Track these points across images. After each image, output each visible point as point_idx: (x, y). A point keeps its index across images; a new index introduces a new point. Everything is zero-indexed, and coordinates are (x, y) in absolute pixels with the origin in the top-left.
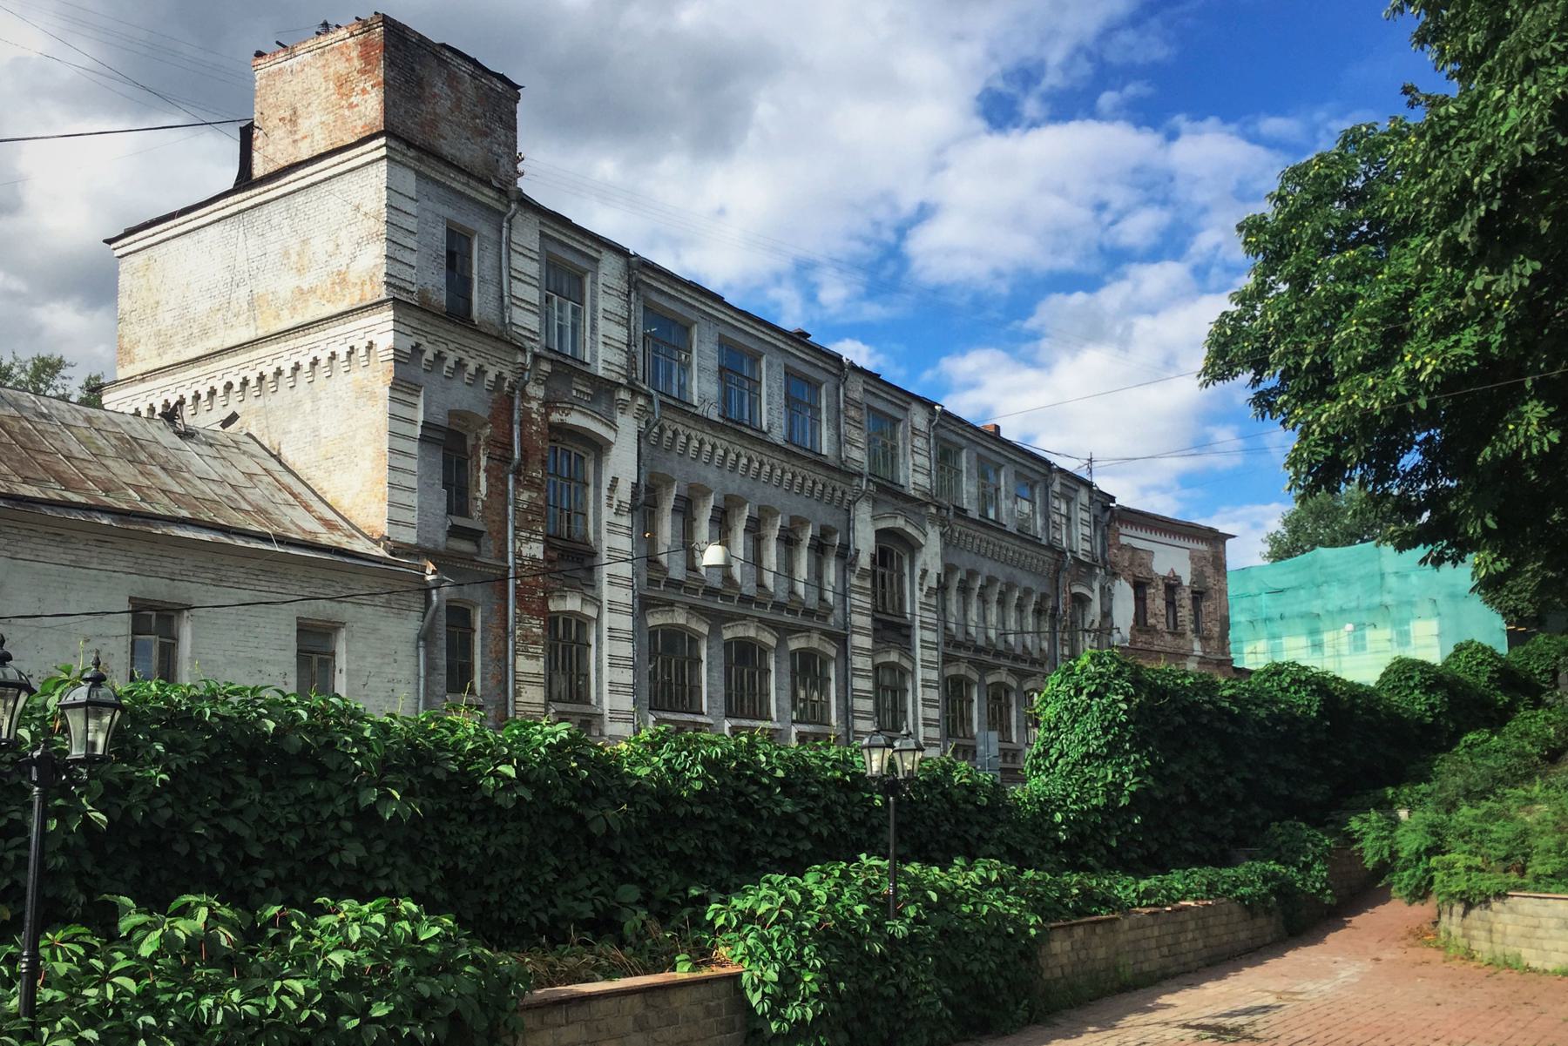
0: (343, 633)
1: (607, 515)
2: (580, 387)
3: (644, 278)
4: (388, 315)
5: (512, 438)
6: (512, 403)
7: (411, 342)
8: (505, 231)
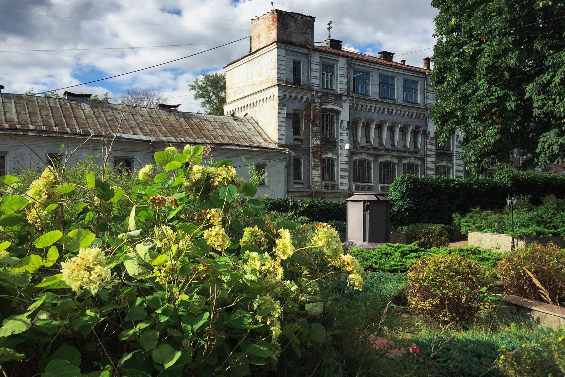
0: (267, 167)
1: (340, 131)
2: (331, 97)
4: (276, 88)
7: (283, 94)
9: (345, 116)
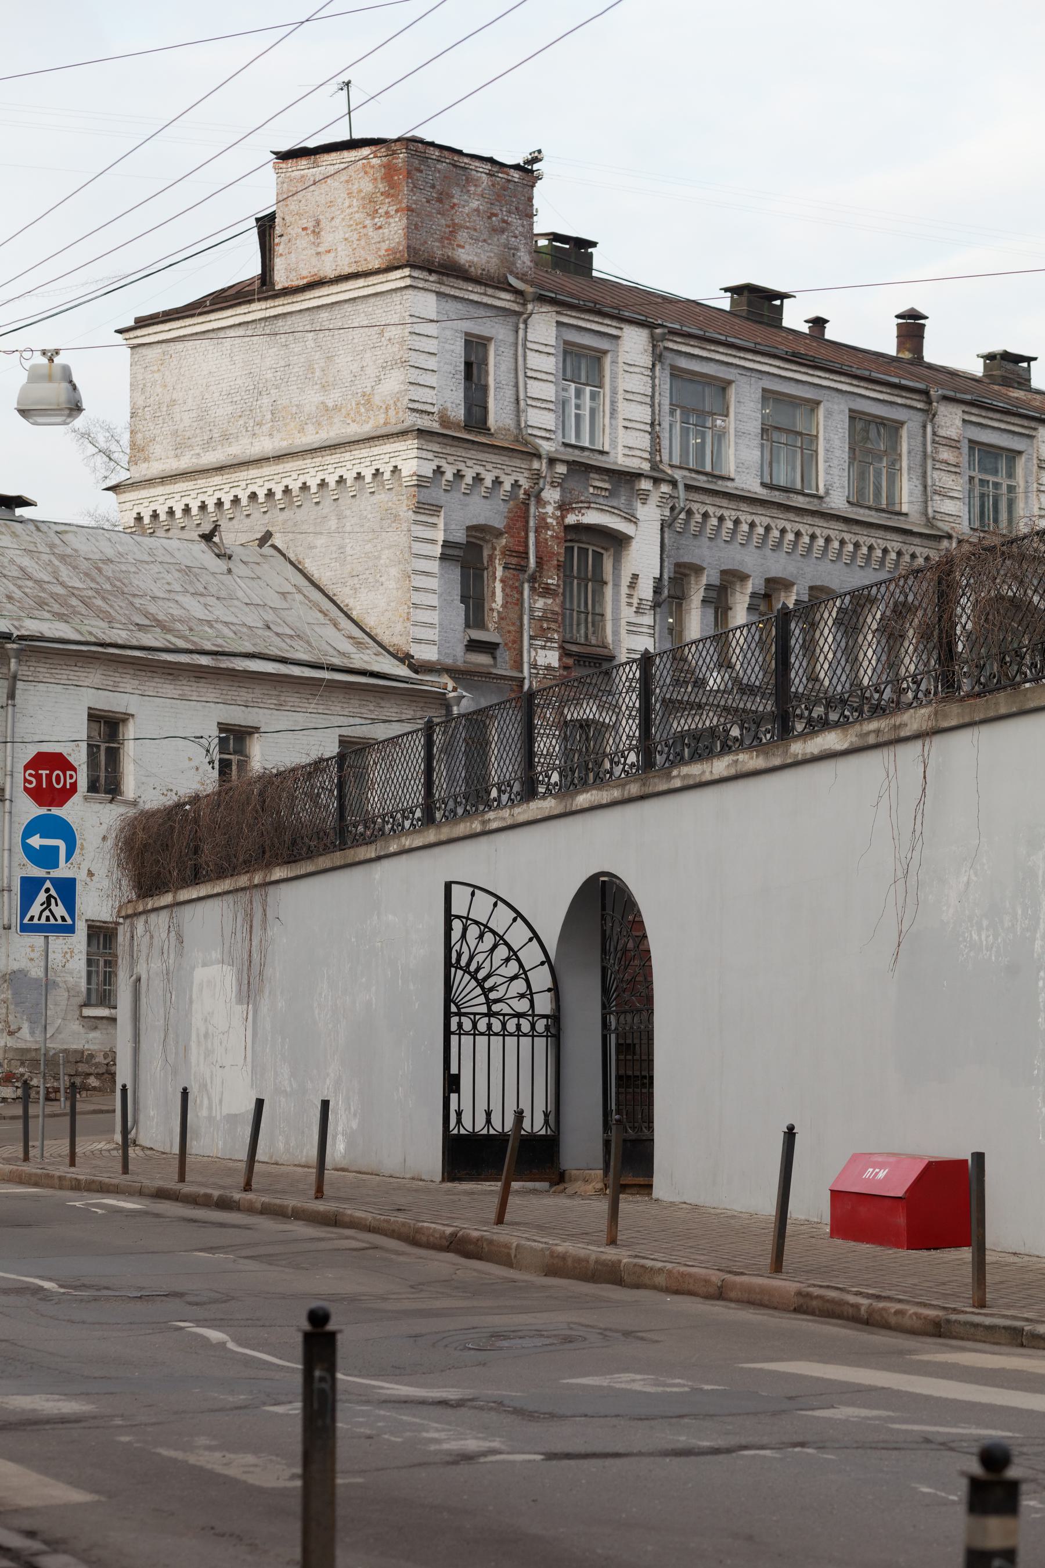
3: (671, 345)
5: (527, 546)
6: (527, 510)
7: (433, 466)
8: (521, 333)
9: (644, 559)
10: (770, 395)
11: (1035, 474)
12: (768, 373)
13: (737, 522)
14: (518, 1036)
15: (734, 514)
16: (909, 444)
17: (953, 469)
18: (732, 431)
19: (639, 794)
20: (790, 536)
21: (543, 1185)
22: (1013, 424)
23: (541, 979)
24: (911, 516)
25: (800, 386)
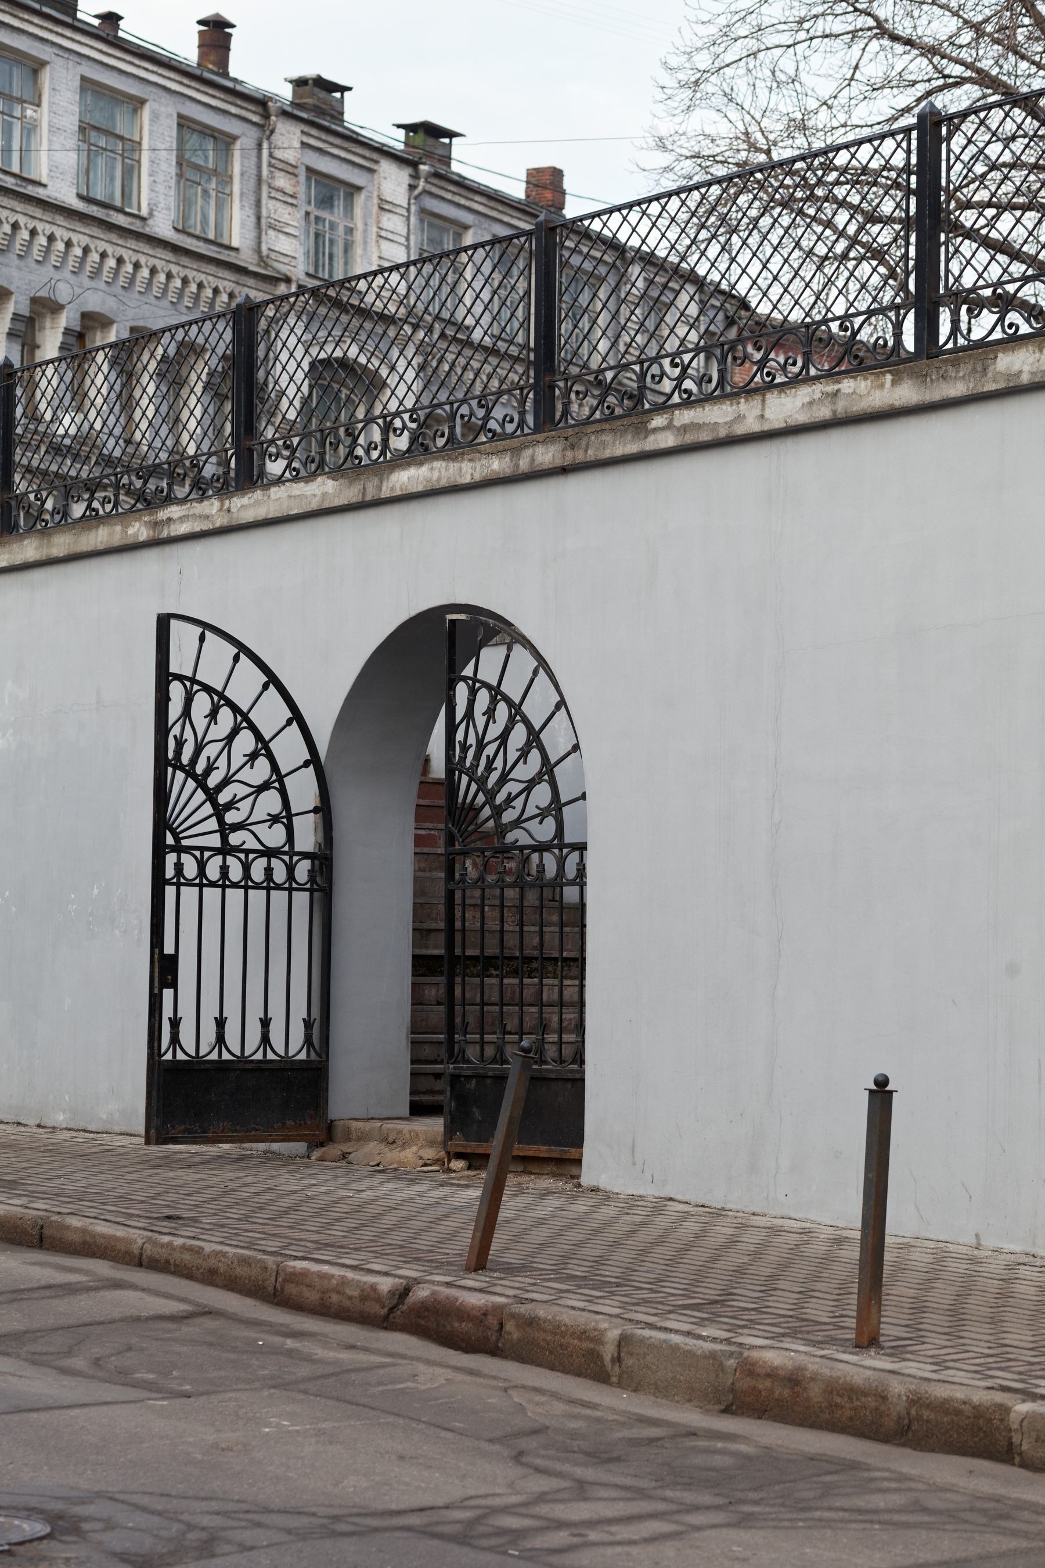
10: (89, 85)
11: (374, 216)
12: (89, 58)
13: (51, 238)
14: (268, 889)
15: (49, 229)
16: (242, 165)
17: (290, 200)
18: (45, 125)
19: (558, 463)
20: (111, 263)
21: (300, 1147)
22: (354, 153)
23: (303, 790)
24: (242, 252)
25: (123, 78)
